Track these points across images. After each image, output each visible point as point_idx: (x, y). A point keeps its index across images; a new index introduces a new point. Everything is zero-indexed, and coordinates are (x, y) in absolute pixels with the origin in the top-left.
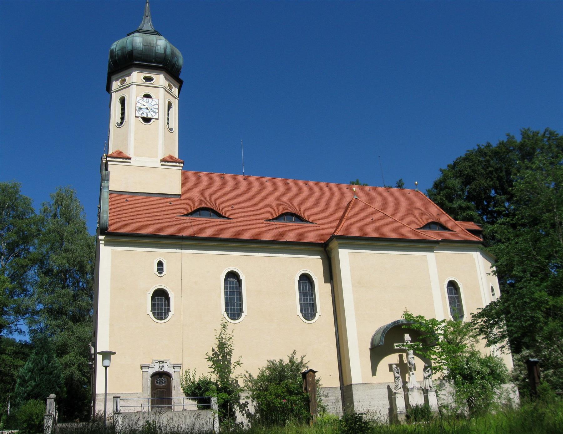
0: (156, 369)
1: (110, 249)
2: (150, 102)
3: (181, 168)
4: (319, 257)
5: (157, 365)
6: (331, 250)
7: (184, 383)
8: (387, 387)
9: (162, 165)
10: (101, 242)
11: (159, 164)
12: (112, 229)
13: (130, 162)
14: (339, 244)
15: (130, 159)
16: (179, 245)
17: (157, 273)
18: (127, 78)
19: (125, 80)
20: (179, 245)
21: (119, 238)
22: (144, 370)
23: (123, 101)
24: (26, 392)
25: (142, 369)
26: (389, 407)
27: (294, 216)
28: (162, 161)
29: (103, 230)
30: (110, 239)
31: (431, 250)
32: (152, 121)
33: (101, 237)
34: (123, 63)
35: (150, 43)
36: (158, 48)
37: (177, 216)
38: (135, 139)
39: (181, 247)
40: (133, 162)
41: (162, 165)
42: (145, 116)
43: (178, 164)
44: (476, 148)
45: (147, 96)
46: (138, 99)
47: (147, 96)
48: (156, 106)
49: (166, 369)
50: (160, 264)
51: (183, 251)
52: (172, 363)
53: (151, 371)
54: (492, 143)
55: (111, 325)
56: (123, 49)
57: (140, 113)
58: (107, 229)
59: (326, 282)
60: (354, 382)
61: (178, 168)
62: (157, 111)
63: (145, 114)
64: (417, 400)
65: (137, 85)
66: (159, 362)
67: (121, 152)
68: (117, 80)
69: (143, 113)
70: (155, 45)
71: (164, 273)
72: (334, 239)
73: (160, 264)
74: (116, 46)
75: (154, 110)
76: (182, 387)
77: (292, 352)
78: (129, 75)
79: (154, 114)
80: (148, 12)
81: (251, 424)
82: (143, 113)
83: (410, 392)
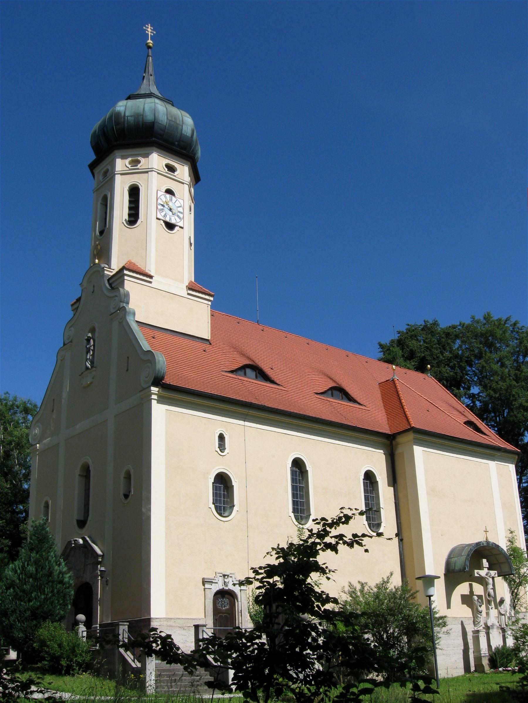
0: (219, 586)
1: (163, 408)
2: (174, 201)
3: (210, 303)
4: (382, 451)
5: (221, 581)
6: (397, 444)
7: (251, 607)
8: (460, 622)
9: (189, 294)
10: (154, 397)
11: (184, 292)
12: (167, 380)
13: (151, 282)
14: (414, 439)
15: (151, 277)
16: (243, 414)
17: (218, 450)
18: (143, 160)
19: (139, 162)
20: (243, 414)
21: (181, 395)
22: (207, 586)
23: (134, 192)
24: (28, 609)
25: (204, 585)
26: (462, 648)
27: (339, 392)
28: (190, 289)
29: (158, 381)
30: (167, 394)
31: (492, 458)
32: (177, 228)
33: (154, 389)
34: (143, 136)
35: (175, 118)
36: (184, 128)
37: (222, 371)
38: (156, 251)
39: (245, 418)
40: (156, 282)
41: (189, 294)
42: (168, 219)
43: (207, 297)
44: (423, 324)
45: (169, 192)
46: (160, 193)
47: (169, 192)
48: (181, 209)
49: (230, 587)
50: (221, 438)
51: (247, 424)
52: (238, 579)
53: (215, 588)
54: (439, 322)
55: (167, 519)
56: (138, 116)
57: (163, 214)
58: (163, 378)
59: (389, 485)
60: (153, 615)
61: (206, 302)
62: (181, 216)
63: (168, 216)
64: (497, 642)
65: (158, 173)
66: (224, 576)
67: (134, 264)
68: (124, 157)
69: (165, 216)
70: (181, 123)
71: (226, 451)
72: (411, 432)
73: (221, 438)
74: (125, 107)
75: (179, 214)
76: (249, 612)
77: (389, 574)
78: (146, 156)
79: (178, 220)
80: (151, 69)
81: (322, 666)
82: (165, 216)
83: (491, 631)
